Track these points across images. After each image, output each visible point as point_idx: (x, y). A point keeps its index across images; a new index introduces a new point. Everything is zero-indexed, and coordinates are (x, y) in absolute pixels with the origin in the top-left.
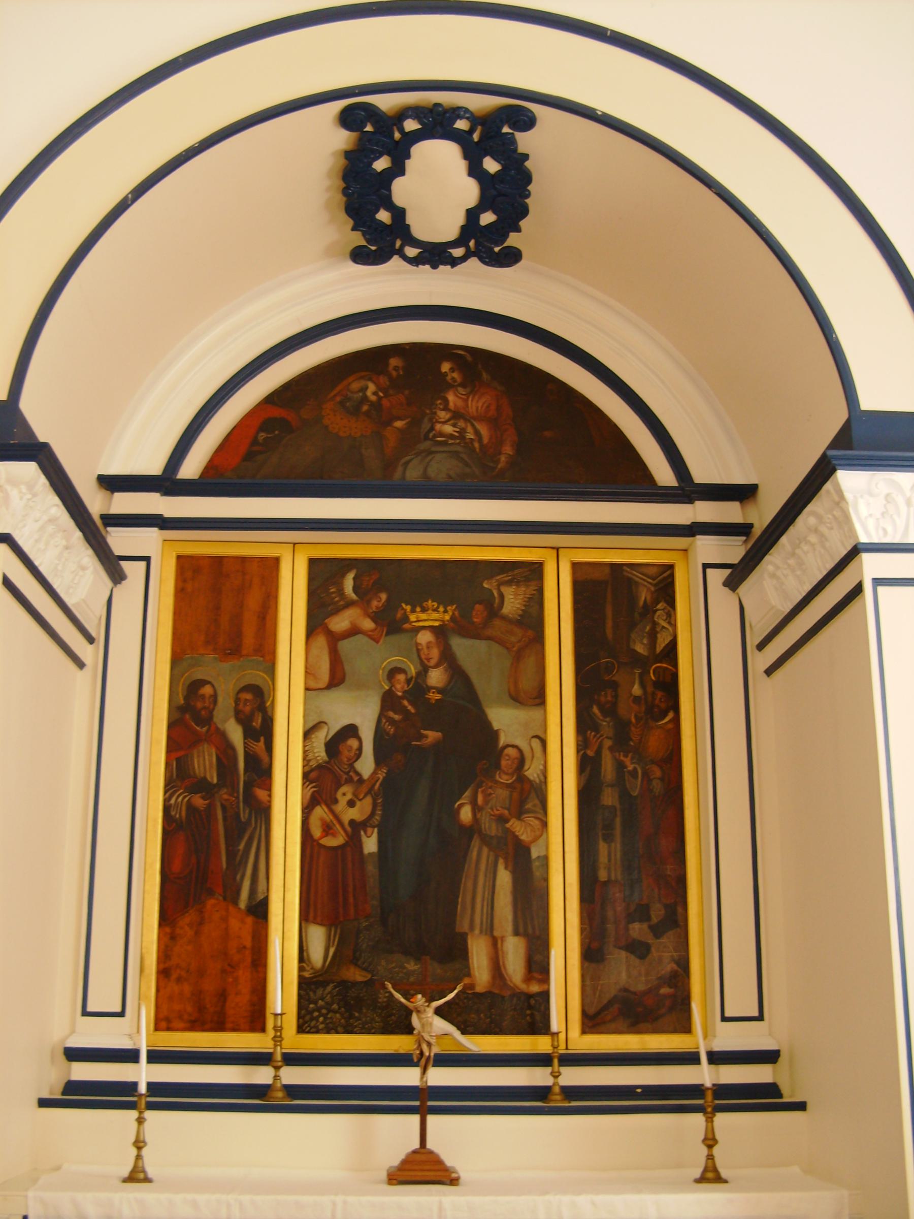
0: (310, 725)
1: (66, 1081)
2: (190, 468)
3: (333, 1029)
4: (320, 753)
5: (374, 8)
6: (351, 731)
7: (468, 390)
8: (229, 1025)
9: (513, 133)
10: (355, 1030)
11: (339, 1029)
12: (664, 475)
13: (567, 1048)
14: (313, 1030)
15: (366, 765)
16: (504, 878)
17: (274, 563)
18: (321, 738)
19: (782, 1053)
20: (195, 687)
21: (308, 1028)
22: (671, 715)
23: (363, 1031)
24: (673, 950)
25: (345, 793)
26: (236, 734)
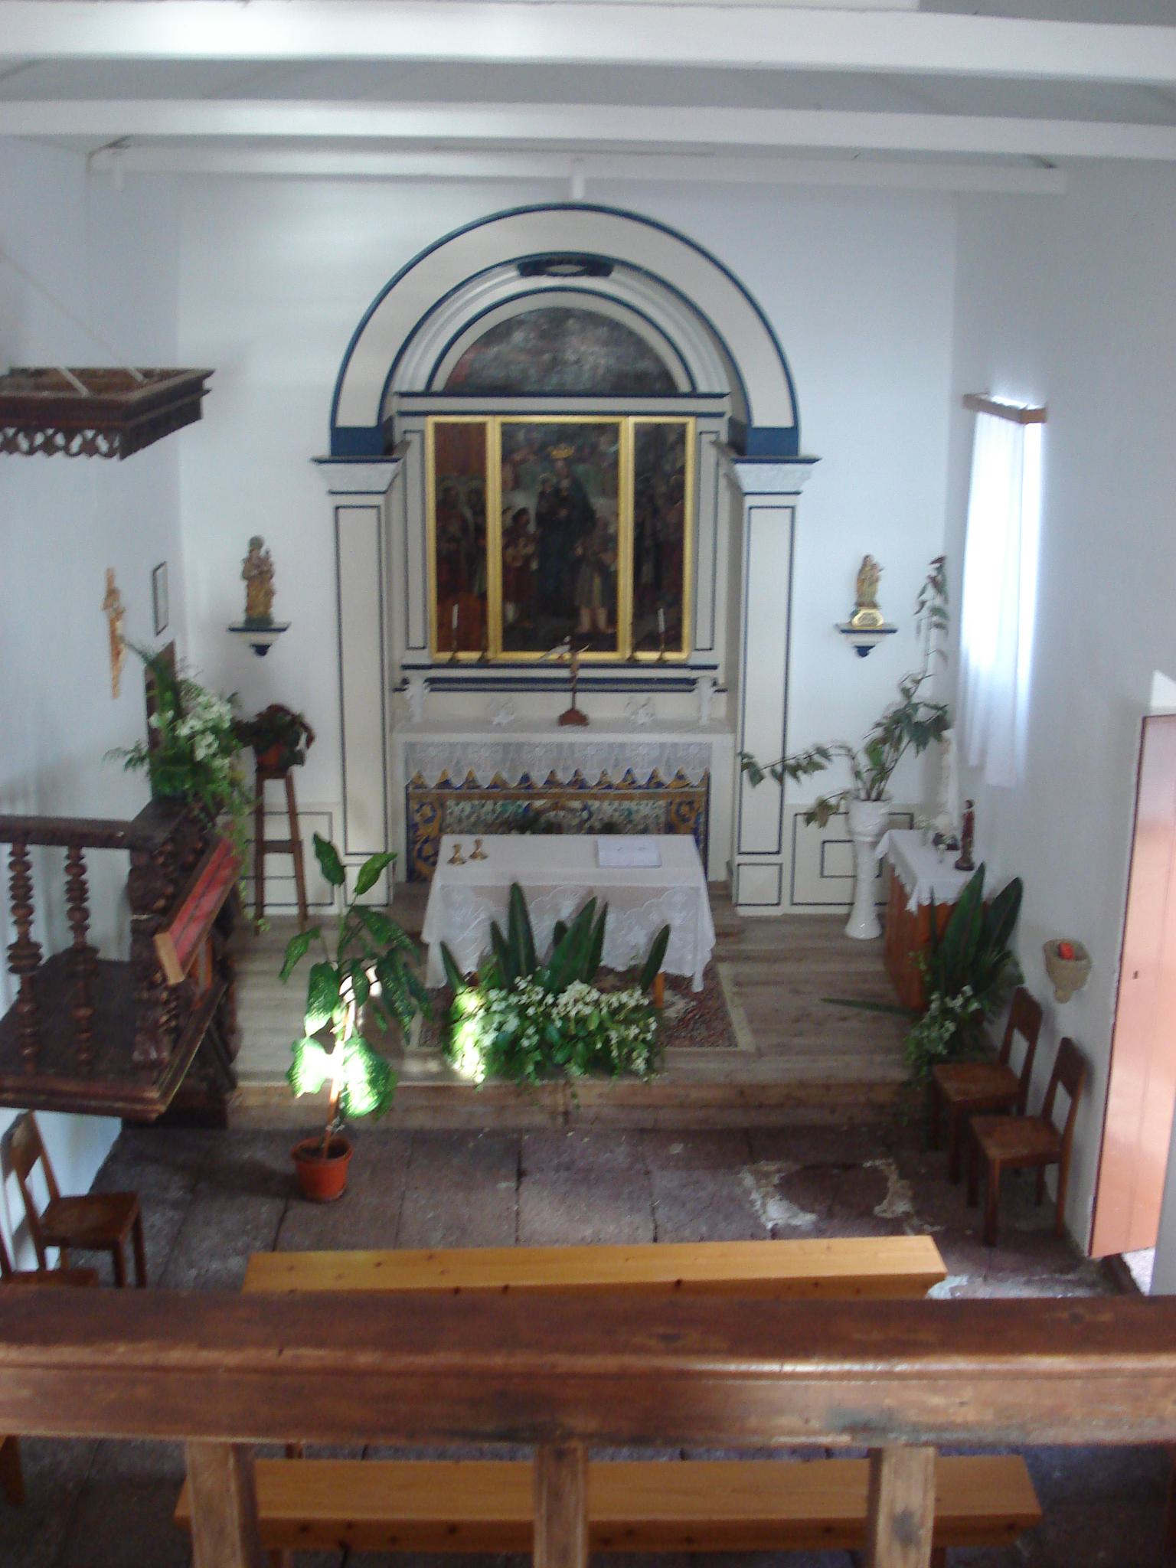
0: (505, 508)
2: (439, 385)
4: (509, 521)
5: (570, 1134)
6: (523, 512)
9: (100, 391)
12: (684, 386)
15: (532, 528)
16: (597, 582)
18: (510, 514)
20: (447, 490)
22: (680, 503)
25: (522, 541)
26: (468, 513)
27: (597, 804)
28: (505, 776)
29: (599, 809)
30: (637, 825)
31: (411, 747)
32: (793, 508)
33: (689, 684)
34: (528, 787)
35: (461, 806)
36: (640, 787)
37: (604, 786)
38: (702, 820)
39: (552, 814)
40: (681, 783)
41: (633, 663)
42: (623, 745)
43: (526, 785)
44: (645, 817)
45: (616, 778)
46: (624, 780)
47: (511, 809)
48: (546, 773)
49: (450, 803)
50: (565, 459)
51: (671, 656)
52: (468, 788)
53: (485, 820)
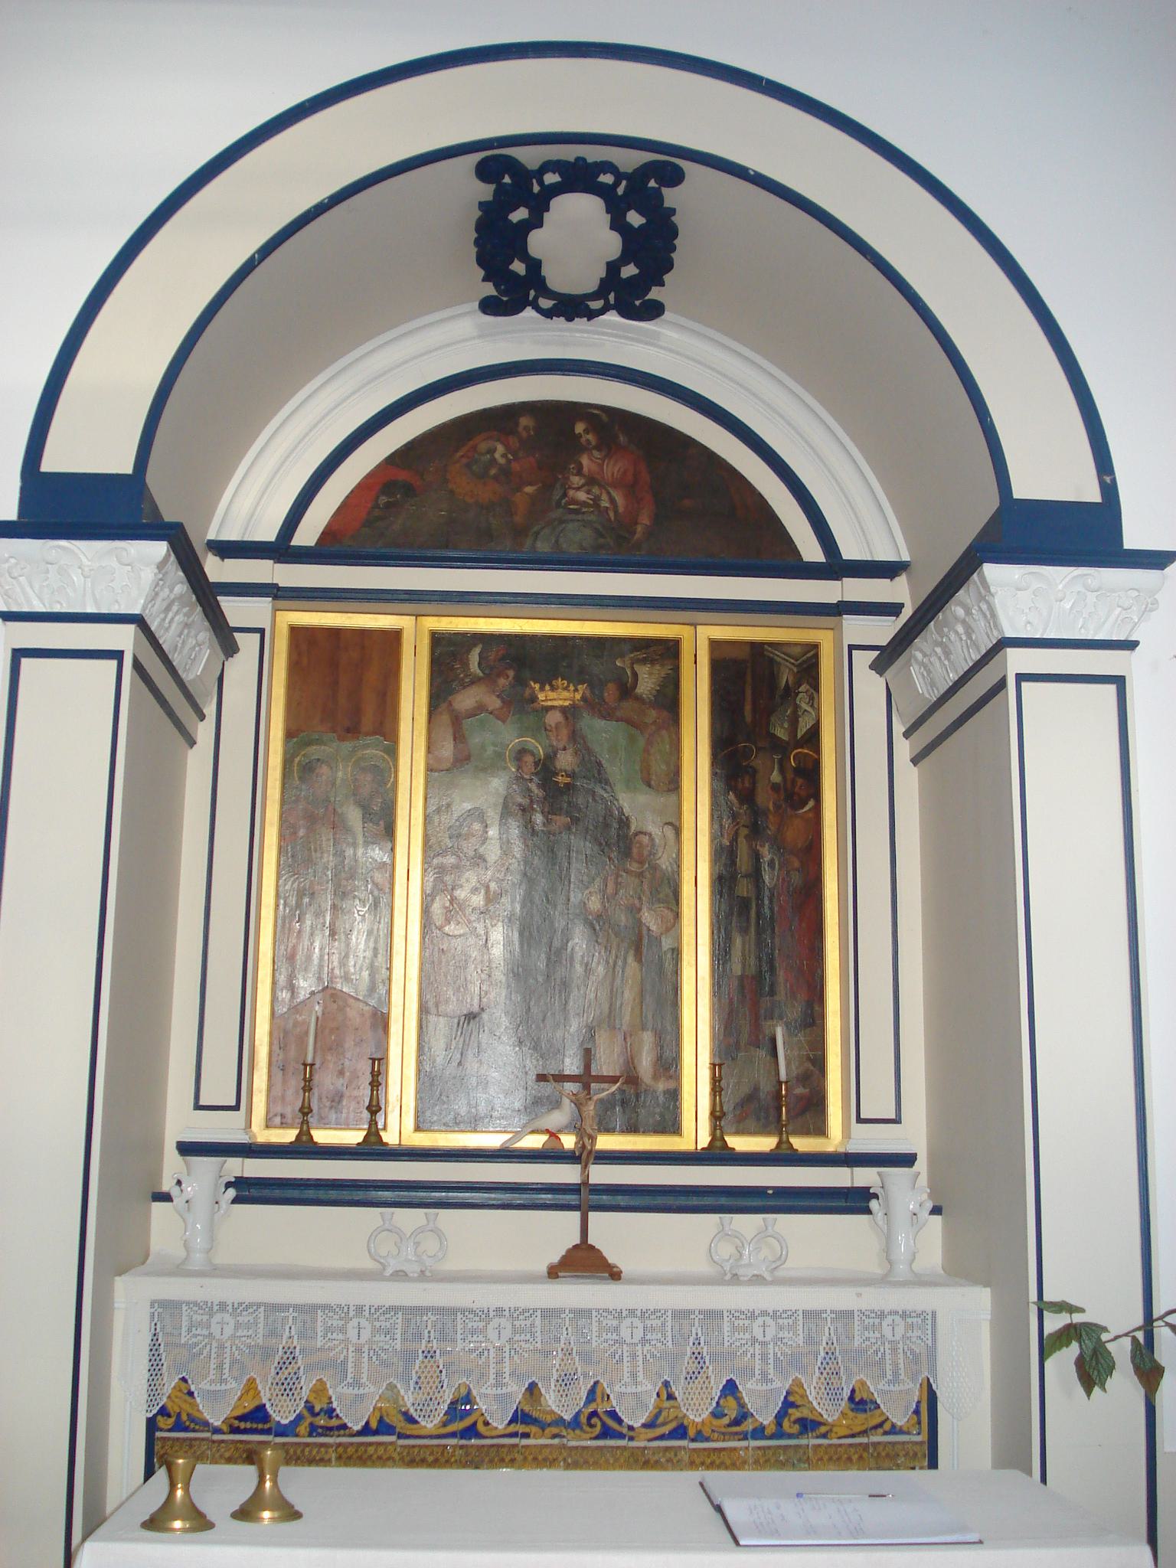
2: (307, 535)
22: (811, 803)
28: (409, 1399)
31: (165, 1309)
32: (1119, 681)
33: (856, 1201)
34: (471, 1431)
36: (759, 1432)
37: (666, 1430)
40: (861, 1421)
41: (717, 1154)
42: (712, 1316)
45: (697, 1411)
46: (717, 1414)
48: (516, 1391)
50: (563, 710)
51: (801, 1144)
52: (313, 1430)
53: (559, 827)
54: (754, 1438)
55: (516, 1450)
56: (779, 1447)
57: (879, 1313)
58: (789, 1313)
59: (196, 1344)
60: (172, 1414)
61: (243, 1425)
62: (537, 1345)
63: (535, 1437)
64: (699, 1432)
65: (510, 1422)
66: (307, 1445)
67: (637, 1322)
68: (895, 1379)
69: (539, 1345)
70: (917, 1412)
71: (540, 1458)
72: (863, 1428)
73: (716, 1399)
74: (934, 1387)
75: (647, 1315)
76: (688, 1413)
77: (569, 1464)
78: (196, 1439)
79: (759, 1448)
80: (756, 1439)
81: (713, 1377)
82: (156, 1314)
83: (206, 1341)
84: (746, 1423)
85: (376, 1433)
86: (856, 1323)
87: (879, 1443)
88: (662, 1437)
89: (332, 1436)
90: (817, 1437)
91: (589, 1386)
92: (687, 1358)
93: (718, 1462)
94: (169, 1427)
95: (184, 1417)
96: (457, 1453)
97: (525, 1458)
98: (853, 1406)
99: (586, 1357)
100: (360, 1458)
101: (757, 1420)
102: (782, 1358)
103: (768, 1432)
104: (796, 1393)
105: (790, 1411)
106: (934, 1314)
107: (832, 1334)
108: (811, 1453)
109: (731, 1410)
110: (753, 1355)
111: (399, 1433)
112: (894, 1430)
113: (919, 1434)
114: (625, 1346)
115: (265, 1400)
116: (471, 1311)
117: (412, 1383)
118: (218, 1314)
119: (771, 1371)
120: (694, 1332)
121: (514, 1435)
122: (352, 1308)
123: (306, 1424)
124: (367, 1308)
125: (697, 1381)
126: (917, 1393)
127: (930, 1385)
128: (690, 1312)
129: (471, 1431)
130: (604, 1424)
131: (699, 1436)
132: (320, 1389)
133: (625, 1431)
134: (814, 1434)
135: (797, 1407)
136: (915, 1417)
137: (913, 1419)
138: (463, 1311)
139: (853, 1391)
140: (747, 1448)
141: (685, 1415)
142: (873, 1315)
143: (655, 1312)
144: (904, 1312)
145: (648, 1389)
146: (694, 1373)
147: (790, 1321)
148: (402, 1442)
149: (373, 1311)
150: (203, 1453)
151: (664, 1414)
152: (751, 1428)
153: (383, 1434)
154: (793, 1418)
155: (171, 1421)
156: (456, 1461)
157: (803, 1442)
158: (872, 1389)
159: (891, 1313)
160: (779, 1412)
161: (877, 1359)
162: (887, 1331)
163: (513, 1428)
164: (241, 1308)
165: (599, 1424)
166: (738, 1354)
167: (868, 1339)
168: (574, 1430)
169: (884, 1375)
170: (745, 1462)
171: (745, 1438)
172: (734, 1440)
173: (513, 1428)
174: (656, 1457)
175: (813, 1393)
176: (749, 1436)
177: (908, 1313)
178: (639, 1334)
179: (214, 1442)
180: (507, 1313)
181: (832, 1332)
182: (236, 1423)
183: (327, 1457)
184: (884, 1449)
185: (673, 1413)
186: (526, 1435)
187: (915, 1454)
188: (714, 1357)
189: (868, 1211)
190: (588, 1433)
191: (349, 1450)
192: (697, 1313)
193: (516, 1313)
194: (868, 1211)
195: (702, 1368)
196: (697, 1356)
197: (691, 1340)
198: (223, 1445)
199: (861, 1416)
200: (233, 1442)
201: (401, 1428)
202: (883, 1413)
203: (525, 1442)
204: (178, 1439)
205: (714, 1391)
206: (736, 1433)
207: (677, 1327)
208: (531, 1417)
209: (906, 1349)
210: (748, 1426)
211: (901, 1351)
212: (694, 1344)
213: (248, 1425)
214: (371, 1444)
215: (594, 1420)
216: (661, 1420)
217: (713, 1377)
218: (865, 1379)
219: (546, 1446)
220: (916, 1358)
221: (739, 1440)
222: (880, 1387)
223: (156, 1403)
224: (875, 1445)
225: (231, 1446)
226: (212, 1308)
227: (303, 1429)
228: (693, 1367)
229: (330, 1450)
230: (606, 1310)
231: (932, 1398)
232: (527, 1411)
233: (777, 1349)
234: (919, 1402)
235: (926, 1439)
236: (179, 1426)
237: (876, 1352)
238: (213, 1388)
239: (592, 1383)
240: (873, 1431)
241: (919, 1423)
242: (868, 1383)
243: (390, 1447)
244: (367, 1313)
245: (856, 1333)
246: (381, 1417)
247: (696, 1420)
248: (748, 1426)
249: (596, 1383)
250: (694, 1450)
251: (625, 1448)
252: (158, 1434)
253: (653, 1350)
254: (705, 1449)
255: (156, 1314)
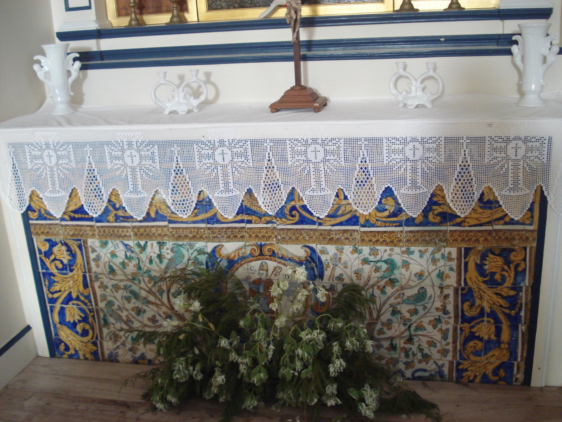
1: (550, 18)
3: (231, 5)
7: (169, 408)
8: (164, 8)
10: (246, 5)
11: (236, 5)
13: (198, 21)
14: (219, 7)
17: (514, 363)
19: (554, 11)
21: (215, 6)
23: (252, 5)
24: (425, 248)
27: (331, 249)
28: (166, 196)
29: (337, 259)
30: (402, 288)
35: (110, 246)
36: (410, 221)
38: (527, 282)
39: (256, 264)
40: (487, 215)
43: (209, 215)
44: (420, 275)
46: (380, 209)
47: (187, 254)
48: (240, 195)
49: (93, 242)
54: (407, 225)
55: (244, 230)
56: (426, 231)
57: (505, 139)
58: (434, 139)
59: (38, 169)
60: (36, 210)
61: (77, 216)
62: (249, 165)
63: (255, 223)
64: (367, 221)
65: (238, 214)
66: (115, 227)
67: (319, 147)
68: (515, 187)
69: (251, 165)
70: (531, 210)
71: (260, 235)
72: (489, 219)
73: (378, 200)
74: (546, 193)
75: (326, 142)
76: (358, 209)
77: (278, 240)
78: (52, 224)
79: (410, 232)
80: (408, 226)
81: (375, 185)
82: (12, 152)
83: (43, 167)
84: (401, 215)
85: (154, 220)
86: (487, 146)
87: (500, 230)
88: (341, 224)
89: (128, 222)
90: (454, 225)
91: (288, 191)
92: (356, 172)
93: (381, 240)
94: (36, 218)
95: (43, 212)
96: (206, 232)
97: (250, 236)
98: (482, 205)
99: (285, 171)
100: (148, 235)
101: (407, 214)
102: (428, 171)
103: (417, 221)
104: (439, 195)
105: (434, 207)
106: (550, 139)
107: (467, 155)
108: (448, 235)
109: (390, 207)
110: (406, 170)
111: (169, 220)
112: (512, 222)
113: (531, 225)
114: (311, 164)
115: (83, 203)
116: (203, 143)
117: (170, 191)
118: (46, 151)
119: (419, 181)
120: (361, 154)
121: (242, 221)
122: (125, 143)
123: (113, 215)
124: (134, 143)
125: (364, 188)
126: (532, 197)
127: (542, 192)
128: (358, 140)
129: (214, 219)
130: (301, 215)
131: (367, 223)
132: (114, 193)
133: (315, 219)
134: (452, 223)
135: (439, 205)
136: (529, 213)
137: (527, 214)
138: (197, 142)
139: (482, 195)
140: (401, 232)
141: (356, 210)
142: (500, 140)
143: (332, 140)
144: (526, 138)
145: (330, 194)
146: (362, 182)
147: (435, 145)
148: (171, 225)
149: (139, 144)
150: (58, 232)
151: (342, 208)
152: (405, 218)
153: (160, 221)
154: (436, 212)
155: (36, 214)
156: (206, 237)
157: (443, 228)
158: (496, 194)
159: (515, 139)
160: (425, 208)
161: (502, 172)
162: (511, 153)
163: (239, 218)
164: (59, 146)
165: (297, 215)
166: (394, 169)
167: (495, 158)
168: (281, 218)
169: (506, 184)
170: (400, 241)
171: (400, 225)
172: (393, 226)
173: (239, 218)
174: (338, 236)
175: (451, 198)
176: (403, 224)
177: (529, 138)
178: (321, 156)
179: (62, 226)
180: (227, 143)
181: (467, 153)
182: (72, 215)
183: (128, 234)
184: (504, 235)
185: (348, 209)
186: (249, 222)
187: (527, 239)
188: (376, 170)
189: (509, 53)
190: (290, 220)
191: (140, 230)
192: (363, 140)
193: (233, 143)
194: (509, 53)
195: (368, 178)
196: (364, 170)
197: (360, 159)
198: (68, 227)
199: (488, 212)
200: (73, 226)
201: (170, 217)
202: (503, 211)
203: (249, 226)
204: (42, 225)
205: (376, 194)
206: (394, 222)
207: (350, 150)
208: (251, 210)
209: (525, 166)
210: (402, 218)
211: (521, 167)
212: (361, 162)
213: (80, 216)
214: (153, 227)
215: (294, 212)
216: (340, 212)
217: (375, 185)
218: (491, 186)
219: (263, 228)
220: (534, 172)
221: (396, 226)
222: (503, 193)
223: (23, 205)
224: (497, 231)
225: (72, 228)
226: (41, 147)
227: (111, 218)
228: (362, 177)
229: (129, 230)
230: (296, 140)
231: (544, 202)
232: (248, 206)
233: (424, 165)
234: (533, 203)
235: (536, 228)
236: (41, 217)
237: (502, 167)
238: (52, 195)
239: (291, 189)
240: (496, 222)
241: (532, 217)
242: (494, 190)
243: (165, 228)
244: (135, 146)
245: (487, 153)
246: (157, 210)
247: (365, 213)
248: (402, 218)
249: (293, 188)
250: (364, 232)
251: (315, 230)
252: (31, 222)
253: (331, 167)
254: (371, 232)
255: (12, 152)
